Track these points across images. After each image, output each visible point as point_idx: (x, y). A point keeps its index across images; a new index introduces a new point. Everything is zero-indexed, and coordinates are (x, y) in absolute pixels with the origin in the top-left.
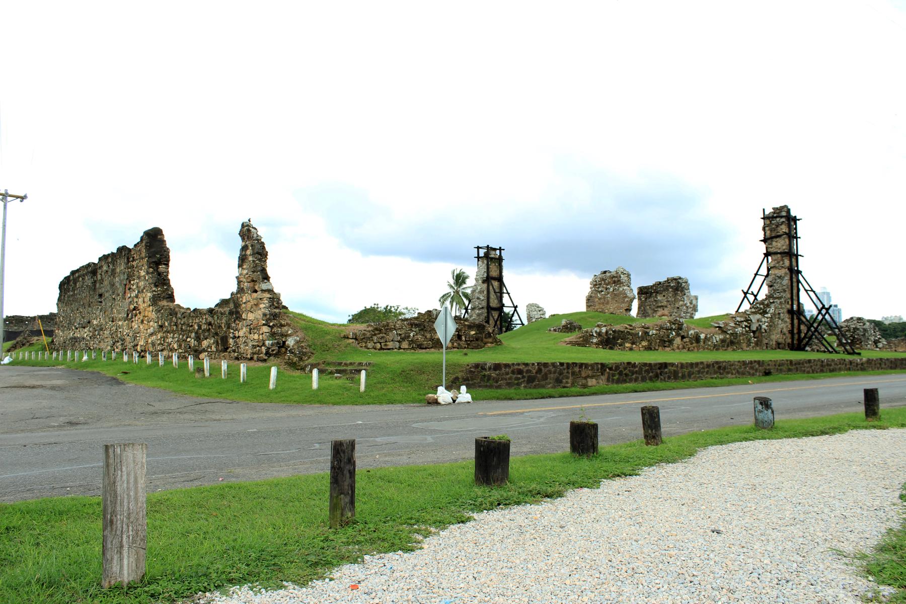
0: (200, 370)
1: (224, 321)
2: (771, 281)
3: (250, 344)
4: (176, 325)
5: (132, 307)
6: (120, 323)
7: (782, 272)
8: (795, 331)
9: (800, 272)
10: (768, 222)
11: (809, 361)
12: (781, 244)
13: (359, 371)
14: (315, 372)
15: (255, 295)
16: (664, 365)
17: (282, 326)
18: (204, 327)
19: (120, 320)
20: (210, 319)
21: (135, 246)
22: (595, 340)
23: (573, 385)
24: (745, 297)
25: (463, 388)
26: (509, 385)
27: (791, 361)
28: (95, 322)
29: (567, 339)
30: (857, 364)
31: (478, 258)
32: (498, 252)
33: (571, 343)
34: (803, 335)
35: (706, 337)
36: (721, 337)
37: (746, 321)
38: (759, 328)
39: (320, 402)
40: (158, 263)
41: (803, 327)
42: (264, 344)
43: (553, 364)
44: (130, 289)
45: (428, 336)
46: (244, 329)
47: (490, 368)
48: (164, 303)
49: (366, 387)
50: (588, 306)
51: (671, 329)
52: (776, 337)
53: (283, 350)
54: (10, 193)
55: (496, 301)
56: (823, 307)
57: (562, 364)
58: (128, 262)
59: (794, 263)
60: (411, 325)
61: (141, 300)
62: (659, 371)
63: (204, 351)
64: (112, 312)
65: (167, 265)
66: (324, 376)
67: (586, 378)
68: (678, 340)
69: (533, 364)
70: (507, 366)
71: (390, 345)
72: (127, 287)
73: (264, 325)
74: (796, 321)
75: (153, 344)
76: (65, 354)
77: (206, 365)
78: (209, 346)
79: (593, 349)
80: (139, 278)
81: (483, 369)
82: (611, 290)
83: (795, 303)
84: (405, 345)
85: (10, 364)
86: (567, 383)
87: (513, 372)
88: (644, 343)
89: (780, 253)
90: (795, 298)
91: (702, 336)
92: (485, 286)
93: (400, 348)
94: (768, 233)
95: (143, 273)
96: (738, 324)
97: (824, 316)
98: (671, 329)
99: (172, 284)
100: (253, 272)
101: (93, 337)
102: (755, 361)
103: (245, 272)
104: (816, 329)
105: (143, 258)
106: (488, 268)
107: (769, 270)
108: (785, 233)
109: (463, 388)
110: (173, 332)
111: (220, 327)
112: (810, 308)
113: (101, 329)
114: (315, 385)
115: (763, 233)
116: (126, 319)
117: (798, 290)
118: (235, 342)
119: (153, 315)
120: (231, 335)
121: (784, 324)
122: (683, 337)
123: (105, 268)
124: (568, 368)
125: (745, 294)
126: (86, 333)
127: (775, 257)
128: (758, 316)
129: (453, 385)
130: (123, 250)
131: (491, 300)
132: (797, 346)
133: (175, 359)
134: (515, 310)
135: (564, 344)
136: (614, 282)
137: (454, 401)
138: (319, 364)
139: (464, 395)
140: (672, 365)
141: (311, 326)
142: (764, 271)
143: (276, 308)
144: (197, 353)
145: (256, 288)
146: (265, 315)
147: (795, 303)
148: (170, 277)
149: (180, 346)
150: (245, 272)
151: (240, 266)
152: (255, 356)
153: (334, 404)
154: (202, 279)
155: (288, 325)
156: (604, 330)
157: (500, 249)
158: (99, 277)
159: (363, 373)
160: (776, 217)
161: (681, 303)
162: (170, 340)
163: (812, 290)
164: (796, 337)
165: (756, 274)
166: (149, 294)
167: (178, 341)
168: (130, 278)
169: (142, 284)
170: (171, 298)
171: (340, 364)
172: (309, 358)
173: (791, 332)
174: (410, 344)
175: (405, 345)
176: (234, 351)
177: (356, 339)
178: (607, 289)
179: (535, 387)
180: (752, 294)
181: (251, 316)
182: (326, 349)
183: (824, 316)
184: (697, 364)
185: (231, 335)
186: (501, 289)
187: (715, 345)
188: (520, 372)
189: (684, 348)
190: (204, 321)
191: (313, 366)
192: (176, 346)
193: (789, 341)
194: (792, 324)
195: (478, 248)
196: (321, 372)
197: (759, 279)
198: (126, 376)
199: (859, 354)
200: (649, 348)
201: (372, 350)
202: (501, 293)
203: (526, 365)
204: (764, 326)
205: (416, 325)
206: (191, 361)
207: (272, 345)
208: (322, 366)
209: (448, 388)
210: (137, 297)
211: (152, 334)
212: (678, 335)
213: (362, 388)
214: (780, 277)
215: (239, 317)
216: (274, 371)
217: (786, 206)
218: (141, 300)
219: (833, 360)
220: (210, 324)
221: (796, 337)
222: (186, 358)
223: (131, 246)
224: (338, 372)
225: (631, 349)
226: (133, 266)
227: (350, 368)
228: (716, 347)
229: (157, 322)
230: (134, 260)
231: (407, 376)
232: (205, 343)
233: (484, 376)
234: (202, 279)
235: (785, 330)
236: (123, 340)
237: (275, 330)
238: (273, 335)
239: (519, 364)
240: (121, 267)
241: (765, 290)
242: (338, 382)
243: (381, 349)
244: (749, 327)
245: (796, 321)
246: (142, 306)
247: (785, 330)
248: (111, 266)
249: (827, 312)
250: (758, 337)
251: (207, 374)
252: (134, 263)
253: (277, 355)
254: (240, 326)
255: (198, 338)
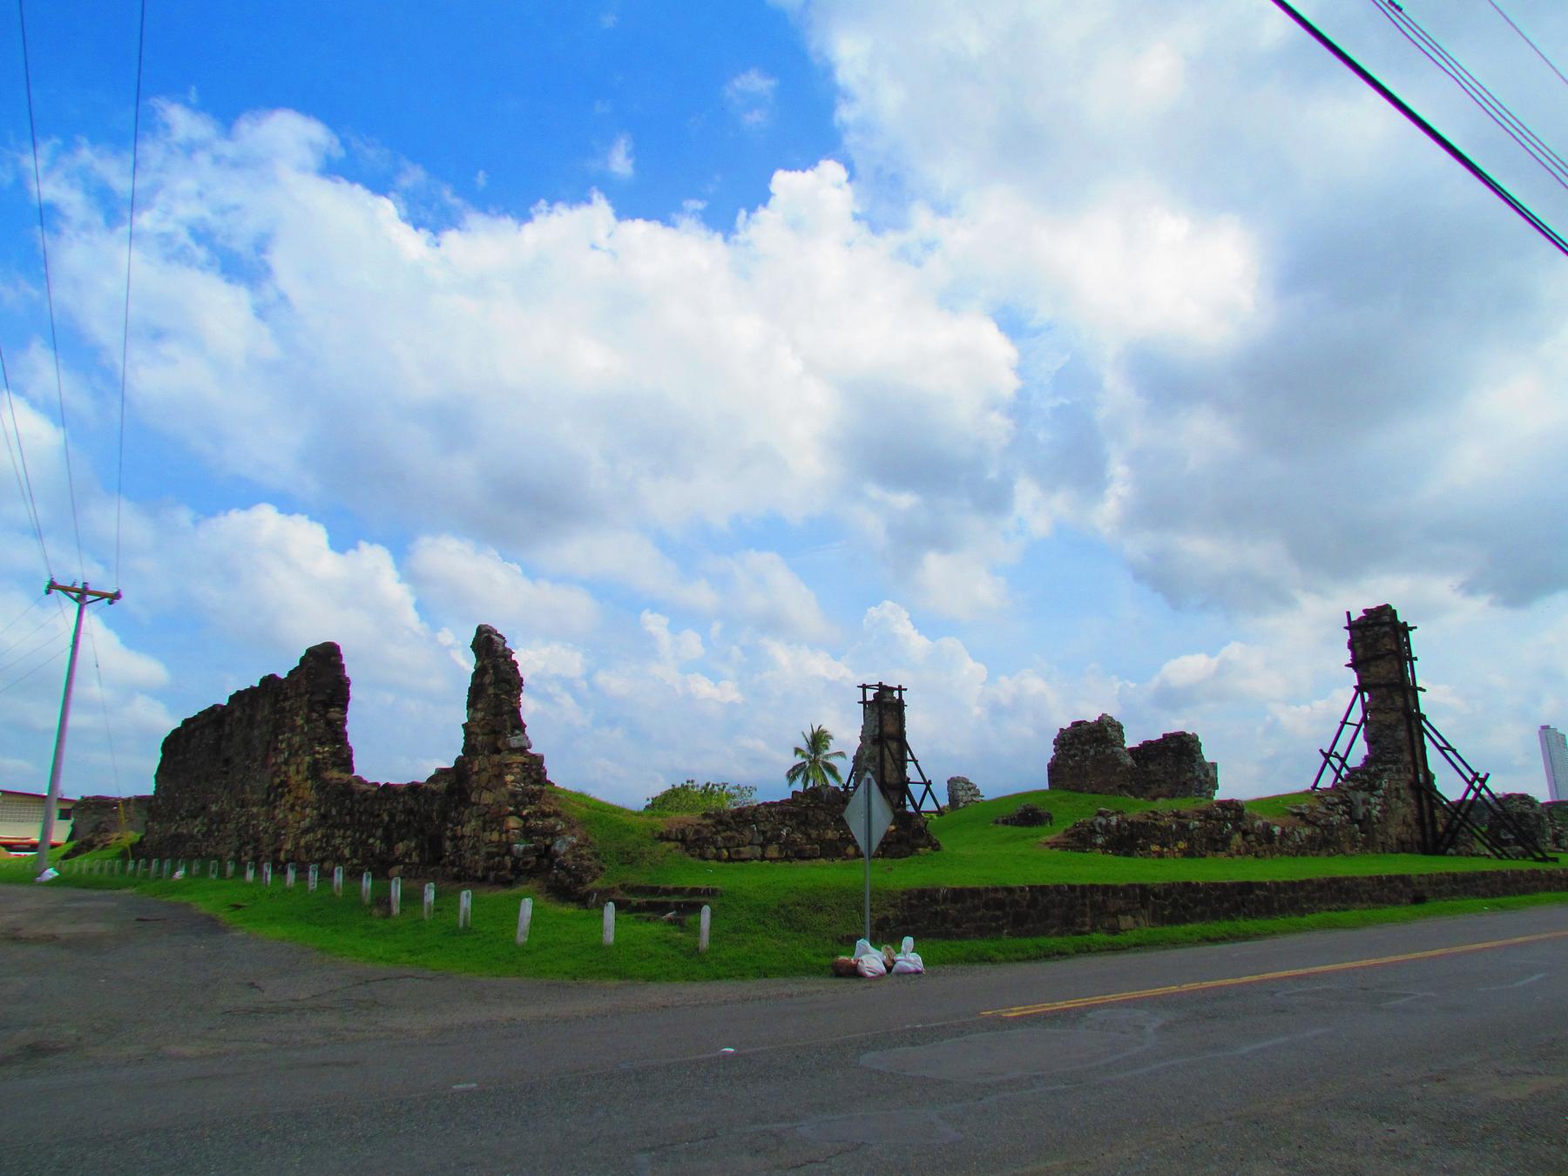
0: (383, 901)
1: (436, 807)
2: (1375, 731)
3: (484, 851)
4: (351, 813)
5: (277, 780)
6: (255, 810)
7: (1390, 718)
8: (1427, 820)
9: (1424, 717)
10: (1358, 634)
11: (1484, 874)
12: (1382, 670)
13: (697, 908)
14: (610, 909)
15: (497, 758)
16: (1247, 887)
17: (545, 815)
18: (400, 817)
19: (254, 805)
20: (411, 803)
21: (291, 673)
22: (1100, 841)
23: (1094, 929)
24: (1327, 761)
25: (908, 941)
26: (982, 932)
27: (1454, 876)
28: (214, 808)
29: (1048, 838)
30: (1561, 879)
31: (864, 702)
32: (896, 694)
33: (1053, 845)
34: (1440, 829)
35: (1283, 832)
36: (1307, 831)
37: (1343, 802)
38: (1368, 814)
39: (621, 975)
40: (326, 705)
41: (1437, 813)
42: (509, 851)
43: (1057, 888)
44: (276, 749)
45: (814, 834)
46: (473, 823)
47: (945, 899)
48: (334, 774)
49: (712, 939)
50: (1051, 781)
51: (1225, 819)
52: (1395, 830)
53: (546, 861)
54: (92, 588)
55: (895, 775)
56: (1476, 775)
57: (1072, 888)
58: (277, 701)
59: (1411, 702)
60: (783, 814)
61: (293, 768)
62: (1239, 898)
63: (397, 862)
64: (243, 791)
65: (345, 708)
66: (624, 917)
67: (1115, 915)
68: (1237, 837)
69: (1022, 889)
70: (975, 892)
71: (746, 851)
72: (271, 747)
73: (511, 814)
74: (1425, 803)
75: (308, 848)
76: (148, 865)
77: (396, 889)
78: (408, 854)
79: (1097, 856)
80: (293, 729)
81: (934, 901)
82: (1092, 752)
83: (1421, 769)
84: (773, 851)
85: (53, 883)
86: (1084, 924)
87: (987, 906)
88: (1182, 845)
89: (1385, 686)
90: (1419, 762)
91: (1277, 830)
92: (877, 749)
93: (763, 858)
94: (1360, 652)
95: (300, 721)
96: (1331, 807)
97: (1478, 791)
98: (1225, 819)
99: (351, 740)
100: (495, 715)
101: (208, 834)
102: (1397, 877)
103: (480, 715)
104: (1465, 816)
105: (301, 695)
106: (881, 721)
107: (1365, 712)
108: (1391, 652)
109: (908, 941)
110: (345, 826)
111: (429, 818)
112: (1450, 787)
113: (222, 821)
114: (609, 937)
115: (1349, 653)
116: (265, 802)
117: (1424, 748)
118: (456, 846)
119: (312, 796)
120: (449, 833)
121: (1405, 809)
122: (1245, 833)
123: (237, 714)
124: (1084, 896)
125: (1327, 756)
126: (197, 827)
127: (1376, 692)
128: (1361, 795)
129: (885, 934)
130: (269, 681)
131: (887, 773)
132: (1433, 844)
133: (339, 878)
134: (928, 788)
135: (1047, 848)
136: (1096, 740)
137: (889, 969)
138: (612, 890)
139: (909, 957)
140: (1261, 885)
141: (601, 817)
142: (1356, 715)
143: (536, 782)
144: (381, 870)
145: (500, 744)
146: (513, 795)
147: (1421, 769)
148: (347, 727)
149: (354, 853)
150: (480, 715)
151: (471, 705)
152: (492, 874)
153: (651, 978)
154: (404, 734)
155: (557, 814)
156: (1114, 820)
157: (900, 689)
158: (227, 729)
159: (706, 909)
160: (1373, 625)
161: (1189, 775)
162: (338, 841)
163: (1449, 748)
164: (1429, 830)
165: (1344, 723)
166: (307, 759)
167: (352, 843)
168: (277, 729)
169: (297, 740)
170: (347, 763)
171: (654, 891)
172: (595, 877)
173: (1420, 821)
174: (781, 851)
175: (773, 851)
176: (453, 864)
177: (683, 841)
178: (1083, 751)
179: (1028, 934)
180: (1337, 755)
181: (487, 798)
182: (628, 858)
183: (1478, 791)
184: (1302, 884)
185: (449, 833)
186: (903, 755)
187: (1300, 847)
188: (999, 905)
189: (1248, 852)
190: (400, 807)
191: (605, 895)
192: (347, 852)
193: (1418, 837)
194: (1420, 808)
195: (864, 687)
196: (619, 906)
197: (1348, 731)
198: (238, 913)
199: (1556, 860)
200: (1188, 854)
201: (714, 863)
202: (903, 761)
203: (1010, 890)
204: (1375, 812)
205: (793, 815)
206: (367, 883)
207: (526, 852)
208: (620, 895)
209: (875, 942)
210: (286, 762)
211: (307, 831)
212: (1236, 828)
213: (704, 941)
214: (1389, 727)
215: (465, 801)
216: (527, 906)
217: (1387, 607)
218: (293, 768)
219: (1521, 873)
220: (410, 812)
221: (1429, 830)
222: (359, 875)
223: (283, 675)
224: (651, 907)
225: (1160, 855)
226: (283, 709)
227: (675, 899)
228: (1300, 851)
229: (318, 808)
230: (286, 699)
231: (792, 915)
232: (401, 847)
233: (936, 913)
234: (404, 734)
235: (1410, 819)
236: (258, 840)
237: (532, 822)
238: (527, 833)
239: (996, 890)
240: (264, 712)
241: (1361, 750)
242: (651, 930)
243: (730, 859)
244: (1349, 814)
245: (1425, 803)
246: (295, 779)
247: (1410, 819)
248: (248, 711)
249: (1483, 785)
250: (1368, 836)
251: (396, 909)
252: (287, 704)
253: (532, 873)
254: (465, 818)
255: (389, 840)
